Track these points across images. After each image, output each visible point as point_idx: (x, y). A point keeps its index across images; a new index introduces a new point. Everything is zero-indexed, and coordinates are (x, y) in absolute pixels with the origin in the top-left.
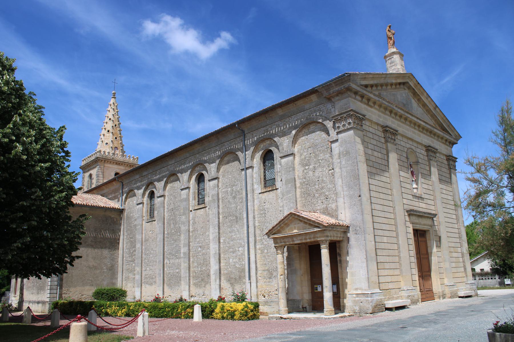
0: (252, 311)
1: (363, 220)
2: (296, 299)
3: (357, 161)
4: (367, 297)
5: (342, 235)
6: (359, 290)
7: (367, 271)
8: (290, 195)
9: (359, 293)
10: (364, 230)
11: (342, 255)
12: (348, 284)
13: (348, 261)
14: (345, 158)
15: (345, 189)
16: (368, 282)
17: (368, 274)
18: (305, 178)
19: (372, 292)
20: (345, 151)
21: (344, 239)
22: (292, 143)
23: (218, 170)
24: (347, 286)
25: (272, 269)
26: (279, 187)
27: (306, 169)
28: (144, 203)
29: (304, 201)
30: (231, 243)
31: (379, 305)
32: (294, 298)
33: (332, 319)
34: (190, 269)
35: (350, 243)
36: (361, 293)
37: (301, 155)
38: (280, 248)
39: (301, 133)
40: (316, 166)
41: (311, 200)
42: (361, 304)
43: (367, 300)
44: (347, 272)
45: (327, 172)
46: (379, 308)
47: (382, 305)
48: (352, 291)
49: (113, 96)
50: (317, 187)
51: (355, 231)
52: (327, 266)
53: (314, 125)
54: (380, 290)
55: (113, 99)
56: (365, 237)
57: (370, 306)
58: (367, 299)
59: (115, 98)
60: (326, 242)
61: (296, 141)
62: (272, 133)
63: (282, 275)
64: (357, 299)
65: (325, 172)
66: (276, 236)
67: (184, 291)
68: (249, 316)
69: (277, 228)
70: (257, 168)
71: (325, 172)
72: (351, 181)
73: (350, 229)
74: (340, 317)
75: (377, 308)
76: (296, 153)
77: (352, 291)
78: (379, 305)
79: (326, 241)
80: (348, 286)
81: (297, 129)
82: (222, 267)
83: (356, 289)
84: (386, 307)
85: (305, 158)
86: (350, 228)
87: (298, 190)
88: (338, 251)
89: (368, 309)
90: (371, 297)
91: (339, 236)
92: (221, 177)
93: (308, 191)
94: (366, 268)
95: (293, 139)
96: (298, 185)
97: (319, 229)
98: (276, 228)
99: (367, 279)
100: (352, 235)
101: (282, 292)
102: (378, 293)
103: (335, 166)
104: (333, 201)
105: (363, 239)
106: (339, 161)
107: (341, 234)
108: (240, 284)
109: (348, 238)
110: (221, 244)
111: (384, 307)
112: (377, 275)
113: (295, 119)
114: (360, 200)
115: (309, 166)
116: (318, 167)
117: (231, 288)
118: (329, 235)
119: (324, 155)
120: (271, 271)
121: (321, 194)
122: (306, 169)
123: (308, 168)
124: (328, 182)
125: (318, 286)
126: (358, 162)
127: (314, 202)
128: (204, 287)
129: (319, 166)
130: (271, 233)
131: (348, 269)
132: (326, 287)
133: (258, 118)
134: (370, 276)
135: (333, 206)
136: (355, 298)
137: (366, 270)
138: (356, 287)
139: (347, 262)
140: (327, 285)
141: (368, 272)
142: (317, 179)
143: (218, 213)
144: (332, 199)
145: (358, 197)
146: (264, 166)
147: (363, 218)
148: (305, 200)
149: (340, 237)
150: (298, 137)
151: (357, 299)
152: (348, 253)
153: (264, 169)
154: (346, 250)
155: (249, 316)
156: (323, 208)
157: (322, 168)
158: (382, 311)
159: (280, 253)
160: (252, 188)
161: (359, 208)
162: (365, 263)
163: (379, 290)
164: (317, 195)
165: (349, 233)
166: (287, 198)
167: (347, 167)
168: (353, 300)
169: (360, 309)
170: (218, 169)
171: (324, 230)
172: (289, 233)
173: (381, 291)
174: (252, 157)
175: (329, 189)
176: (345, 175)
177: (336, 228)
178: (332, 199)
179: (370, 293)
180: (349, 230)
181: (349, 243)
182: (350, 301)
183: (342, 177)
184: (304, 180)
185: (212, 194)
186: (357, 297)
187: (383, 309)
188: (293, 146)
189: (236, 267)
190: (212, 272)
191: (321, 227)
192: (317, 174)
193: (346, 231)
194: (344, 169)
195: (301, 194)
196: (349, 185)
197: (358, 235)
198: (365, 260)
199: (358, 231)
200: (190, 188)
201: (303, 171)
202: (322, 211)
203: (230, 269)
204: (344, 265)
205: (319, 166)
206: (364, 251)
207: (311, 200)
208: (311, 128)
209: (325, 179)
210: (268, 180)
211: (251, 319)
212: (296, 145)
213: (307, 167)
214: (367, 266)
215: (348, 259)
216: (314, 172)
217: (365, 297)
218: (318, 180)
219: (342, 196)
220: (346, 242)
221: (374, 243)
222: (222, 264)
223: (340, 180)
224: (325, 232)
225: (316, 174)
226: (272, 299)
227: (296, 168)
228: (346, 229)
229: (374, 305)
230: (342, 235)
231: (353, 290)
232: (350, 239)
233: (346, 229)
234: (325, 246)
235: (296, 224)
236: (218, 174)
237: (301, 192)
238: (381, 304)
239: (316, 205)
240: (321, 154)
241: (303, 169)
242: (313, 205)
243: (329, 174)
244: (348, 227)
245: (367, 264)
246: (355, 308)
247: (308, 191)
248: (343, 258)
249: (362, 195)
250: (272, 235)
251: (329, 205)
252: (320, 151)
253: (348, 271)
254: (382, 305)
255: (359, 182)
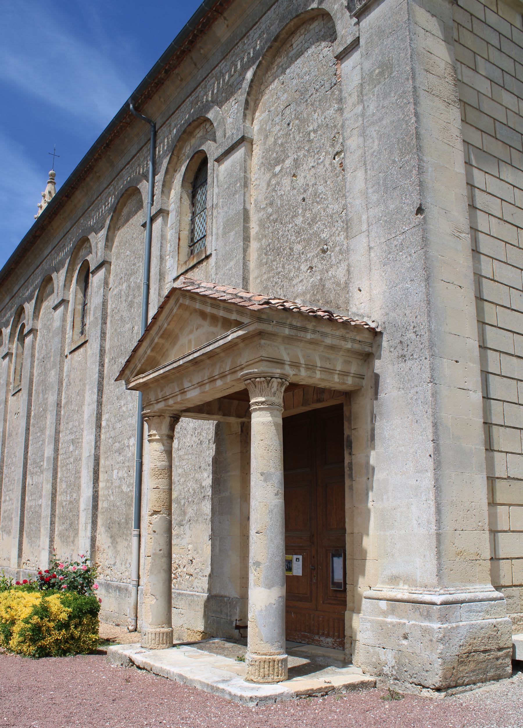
0: (65, 625)
1: (429, 303)
2: (227, 594)
3: (414, 88)
4: (428, 617)
5: (353, 369)
6: (405, 583)
7: (433, 510)
8: (232, 263)
9: (399, 596)
10: (430, 340)
11: (353, 445)
12: (370, 556)
13: (373, 469)
14: (376, 89)
15: (374, 198)
16: (439, 555)
17: (439, 522)
18: (271, 204)
19: (450, 598)
20: (379, 68)
21: (364, 382)
22: (246, 109)
23: (109, 244)
24: (364, 566)
25: (184, 498)
26: (213, 249)
27: (275, 175)
28: (12, 354)
29: (266, 276)
30: (118, 425)
31: (485, 651)
32: (222, 593)
33: (252, 705)
34: (56, 496)
35: (381, 395)
36: (406, 596)
37: (266, 137)
38: (156, 420)
39: (269, 74)
40: (301, 154)
41: (283, 267)
42: (405, 642)
43: (426, 631)
44: (369, 511)
45: (327, 165)
46: (484, 666)
47: (500, 649)
48: (379, 586)
49: (49, 180)
50: (299, 220)
51: (399, 346)
52: (265, 480)
53: (302, 31)
54: (498, 588)
55: (50, 184)
56: (432, 369)
57: (435, 656)
58: (426, 624)
59: (55, 183)
60: (268, 382)
61: (257, 102)
62: (207, 101)
63: (155, 512)
64: (391, 619)
65: (322, 166)
66: (141, 381)
67: (43, 551)
68: (48, 641)
69: (145, 352)
70: (174, 213)
71: (322, 166)
72: (394, 162)
73: (385, 344)
74: (298, 695)
75: (472, 666)
76: (255, 138)
77: (379, 586)
78: (485, 651)
79: (268, 379)
80: (370, 566)
81: (258, 62)
82: (101, 493)
83: (394, 580)
84: (518, 658)
85: (275, 143)
86: (385, 338)
87: (254, 245)
88: (346, 432)
89: (428, 667)
90: (444, 618)
91: (339, 367)
92: (113, 260)
93: (276, 242)
94: (432, 496)
95: (249, 94)
96: (254, 228)
97: (240, 333)
98: (141, 351)
99: (434, 540)
100: (390, 366)
101: (151, 571)
102: (480, 601)
103: (349, 130)
104: (340, 257)
105: (426, 375)
106: (359, 109)
107: (347, 362)
108: (126, 540)
109: (377, 377)
110: (103, 431)
111: (509, 661)
112: (487, 527)
113: (256, 36)
114: (423, 226)
115: (283, 161)
116: (305, 156)
117: (112, 548)
118: (286, 358)
119: (323, 113)
120: (183, 502)
121: (308, 241)
122: (275, 175)
123: (281, 171)
124: (329, 193)
125: (295, 557)
126: (421, 93)
127: (290, 271)
128: (73, 542)
129: (308, 151)
130: (132, 373)
131: (370, 499)
132: (257, 564)
133: (176, 71)
134: (448, 527)
135: (340, 273)
136: (385, 614)
137: (432, 503)
138: (395, 571)
139: (370, 471)
140: (259, 558)
141: (438, 511)
142: (302, 197)
143: (101, 350)
144: (337, 249)
145: (413, 217)
146: (193, 204)
147: (428, 295)
148: (269, 272)
149: (344, 374)
150: (263, 87)
151: (391, 619)
152: (373, 438)
153: (193, 213)
154: (369, 428)
155: (48, 641)
156: (313, 286)
157: (316, 156)
158: (497, 678)
159: (157, 437)
160: (158, 267)
161: (414, 256)
162: (430, 474)
163: (490, 587)
164: (298, 248)
165: (379, 358)
166: (224, 274)
167: (381, 120)
168: (377, 622)
169: (399, 663)
170: (109, 240)
171: (261, 334)
172: (166, 364)
173: (497, 594)
174: (166, 185)
175: (332, 217)
176: (375, 147)
177: (314, 332)
178: (337, 249)
179: (438, 599)
180: (380, 346)
181: (376, 399)
182: (368, 625)
183: (365, 164)
184: (270, 210)
185: (94, 306)
186: (392, 611)
187: (503, 667)
188: (249, 117)
189: (122, 491)
190: (82, 506)
191: (245, 320)
192: (302, 180)
193: (367, 349)
194: (372, 131)
195: (260, 256)
196: (385, 180)
197: (409, 363)
198: (430, 463)
199: (411, 349)
200: (68, 301)
201: (269, 184)
202: (308, 296)
203: (112, 498)
204: (359, 482)
205: (308, 151)
206: (429, 424)
207: (283, 267)
208: (294, 46)
209: (321, 188)
210: (198, 241)
211: (54, 651)
212: (257, 114)
213: (278, 169)
214: (438, 488)
215: (372, 462)
216: (294, 175)
217: (421, 614)
218: (304, 200)
219: (364, 227)
220: (370, 393)
221: (477, 397)
222: (101, 485)
223: (360, 174)
224: (263, 342)
225: (300, 181)
226: (181, 587)
227: (253, 179)
228: (371, 345)
229: (455, 650)
230: (353, 369)
231: (383, 582)
232: (381, 380)
233: (371, 345)
234: (263, 399)
235: (191, 332)
236: (108, 252)
237: (261, 249)
238: (495, 647)
239: (294, 282)
240: (315, 111)
241: (268, 176)
242: (286, 284)
243: (334, 168)
244: (375, 334)
245: (437, 480)
246: (383, 658)
247: (276, 242)
248: (358, 457)
249: (432, 211)
250: (136, 375)
251: (330, 273)
252: (312, 105)
253: (370, 504)
254: (500, 649)
255: (420, 160)
